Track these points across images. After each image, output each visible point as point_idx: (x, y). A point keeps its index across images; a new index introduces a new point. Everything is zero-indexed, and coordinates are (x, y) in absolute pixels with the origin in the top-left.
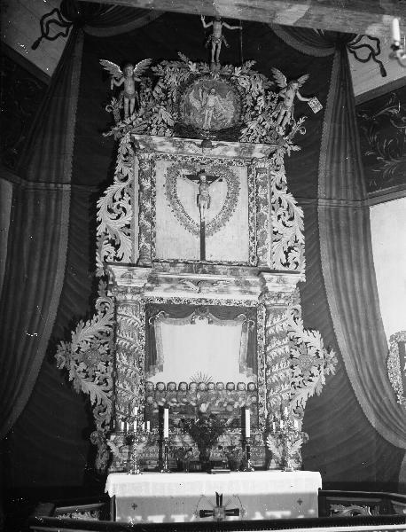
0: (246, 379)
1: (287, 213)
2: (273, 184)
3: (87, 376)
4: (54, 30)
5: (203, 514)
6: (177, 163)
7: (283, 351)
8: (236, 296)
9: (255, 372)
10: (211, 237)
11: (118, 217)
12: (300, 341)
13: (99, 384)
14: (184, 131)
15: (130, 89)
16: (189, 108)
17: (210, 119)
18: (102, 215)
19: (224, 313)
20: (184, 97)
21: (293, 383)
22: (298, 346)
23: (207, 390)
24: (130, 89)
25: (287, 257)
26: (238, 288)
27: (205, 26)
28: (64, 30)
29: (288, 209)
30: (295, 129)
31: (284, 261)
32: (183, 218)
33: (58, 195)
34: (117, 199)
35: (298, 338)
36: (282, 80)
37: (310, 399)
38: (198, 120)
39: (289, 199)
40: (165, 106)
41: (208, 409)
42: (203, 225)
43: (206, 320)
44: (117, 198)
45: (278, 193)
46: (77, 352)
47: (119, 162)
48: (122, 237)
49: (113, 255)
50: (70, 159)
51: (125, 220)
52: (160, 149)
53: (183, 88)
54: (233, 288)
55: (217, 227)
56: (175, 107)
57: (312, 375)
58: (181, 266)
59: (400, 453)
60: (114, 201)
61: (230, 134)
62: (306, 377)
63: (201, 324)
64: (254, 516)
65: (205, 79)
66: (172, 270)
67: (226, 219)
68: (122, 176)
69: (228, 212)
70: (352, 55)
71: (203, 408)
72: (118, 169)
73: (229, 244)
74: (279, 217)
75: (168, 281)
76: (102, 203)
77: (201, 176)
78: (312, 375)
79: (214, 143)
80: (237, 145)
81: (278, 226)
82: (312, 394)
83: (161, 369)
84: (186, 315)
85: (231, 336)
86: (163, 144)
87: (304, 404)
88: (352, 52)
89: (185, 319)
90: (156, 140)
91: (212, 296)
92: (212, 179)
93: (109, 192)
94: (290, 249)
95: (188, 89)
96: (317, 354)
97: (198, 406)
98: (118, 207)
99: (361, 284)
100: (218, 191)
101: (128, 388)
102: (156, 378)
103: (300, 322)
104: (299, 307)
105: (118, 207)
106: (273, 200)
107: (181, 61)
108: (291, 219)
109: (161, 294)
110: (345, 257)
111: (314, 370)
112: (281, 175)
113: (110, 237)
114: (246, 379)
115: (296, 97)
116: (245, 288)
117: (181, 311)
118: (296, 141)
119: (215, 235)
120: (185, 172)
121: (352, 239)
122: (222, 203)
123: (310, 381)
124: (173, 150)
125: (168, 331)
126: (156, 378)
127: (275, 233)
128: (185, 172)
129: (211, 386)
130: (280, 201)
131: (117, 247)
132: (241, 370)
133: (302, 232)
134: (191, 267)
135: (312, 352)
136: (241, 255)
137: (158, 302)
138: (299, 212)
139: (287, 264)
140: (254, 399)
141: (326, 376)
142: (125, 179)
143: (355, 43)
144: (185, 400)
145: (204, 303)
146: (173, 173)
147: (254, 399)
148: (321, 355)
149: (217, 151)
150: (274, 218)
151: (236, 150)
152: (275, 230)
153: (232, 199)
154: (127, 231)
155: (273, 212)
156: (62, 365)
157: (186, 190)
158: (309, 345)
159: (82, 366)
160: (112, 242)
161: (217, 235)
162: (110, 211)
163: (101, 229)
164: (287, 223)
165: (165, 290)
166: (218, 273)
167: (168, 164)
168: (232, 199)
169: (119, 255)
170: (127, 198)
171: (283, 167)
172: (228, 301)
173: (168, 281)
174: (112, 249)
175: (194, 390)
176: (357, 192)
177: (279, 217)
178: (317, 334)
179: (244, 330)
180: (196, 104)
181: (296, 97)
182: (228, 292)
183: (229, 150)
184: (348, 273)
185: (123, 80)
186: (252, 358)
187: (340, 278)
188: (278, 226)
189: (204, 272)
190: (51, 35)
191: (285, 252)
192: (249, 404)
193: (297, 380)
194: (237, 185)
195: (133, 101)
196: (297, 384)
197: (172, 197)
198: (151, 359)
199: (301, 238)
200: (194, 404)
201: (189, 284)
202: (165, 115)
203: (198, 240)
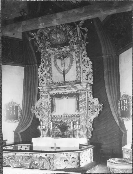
0: (77, 113)
1: (87, 63)
2: (82, 55)
3: (38, 114)
5: (52, 148)
6: (56, 55)
7: (82, 106)
8: (73, 91)
10: (66, 75)
11: (43, 73)
12: (92, 102)
13: (41, 116)
14: (53, 46)
15: (37, 39)
16: (53, 39)
17: (60, 41)
18: (39, 73)
19: (70, 95)
20: (51, 37)
21: (90, 114)
22: (91, 103)
24: (37, 39)
25: (87, 77)
26: (73, 88)
29: (87, 62)
31: (86, 78)
33: (35, 67)
37: (94, 119)
38: (57, 42)
39: (88, 59)
40: (47, 40)
41: (67, 122)
42: (64, 71)
43: (66, 98)
45: (84, 58)
46: (36, 108)
47: (42, 58)
49: (42, 83)
50: (35, 58)
51: (44, 73)
52: (49, 52)
53: (49, 35)
54: (72, 88)
55: (68, 71)
56: (49, 40)
57: (95, 112)
58: (57, 84)
60: (42, 68)
61: (66, 44)
62: (93, 112)
63: (65, 99)
64: (129, 150)
65: (53, 31)
66: (54, 86)
67: (70, 68)
68: (43, 61)
69: (71, 66)
71: (65, 121)
72: (42, 60)
73: (71, 76)
74: (85, 65)
75: (55, 88)
77: (63, 57)
78: (95, 112)
79: (62, 48)
80: (68, 47)
81: (84, 68)
82: (95, 117)
83: (55, 111)
84: (61, 97)
85: (73, 101)
86: (50, 50)
87: (93, 120)
89: (61, 98)
90: (48, 50)
91: (67, 91)
94: (89, 74)
95: (51, 34)
96: (97, 105)
97: (64, 121)
98: (43, 70)
99: (114, 81)
100: (68, 60)
101: (44, 117)
102: (55, 114)
103: (92, 96)
104: (91, 92)
105: (43, 70)
106: (82, 60)
109: (55, 92)
110: (112, 73)
111: (96, 110)
112: (84, 52)
113: (41, 78)
116: (75, 88)
117: (60, 96)
118: (87, 40)
119: (67, 73)
120: (58, 57)
122: (69, 64)
123: (95, 113)
124: (53, 52)
125: (57, 101)
126: (55, 114)
127: (84, 70)
128: (58, 57)
130: (85, 60)
131: (43, 81)
132: (76, 111)
133: (92, 69)
134: (60, 84)
135: (95, 105)
136: (74, 78)
137: (54, 94)
138: (91, 62)
139: (87, 79)
140: (78, 119)
141: (99, 111)
142: (43, 62)
144: (61, 119)
145: (65, 93)
146: (55, 58)
147: (78, 119)
148: (98, 105)
149: (64, 50)
150: (83, 66)
151: (69, 48)
152: (83, 69)
153: (71, 62)
154: (45, 76)
155: (83, 64)
157: (59, 62)
158: (94, 103)
159: (37, 112)
160: (42, 80)
161: (68, 73)
162: (41, 71)
165: (55, 91)
166: (66, 85)
167: (54, 55)
168: (71, 62)
169: (44, 83)
170: (44, 67)
171: (85, 50)
172: (71, 92)
173: (55, 88)
174: (42, 81)
177: (85, 65)
178: (97, 99)
179: (76, 100)
180: (54, 38)
182: (71, 90)
183: (68, 48)
184: (112, 78)
185: (35, 37)
187: (110, 80)
188: (84, 68)
189: (62, 85)
192: (77, 120)
193: (90, 113)
194: (73, 58)
195: (39, 41)
196: (91, 114)
197: (56, 64)
199: (91, 71)
200: (63, 121)
201: (61, 89)
202: (48, 43)
203: (63, 76)
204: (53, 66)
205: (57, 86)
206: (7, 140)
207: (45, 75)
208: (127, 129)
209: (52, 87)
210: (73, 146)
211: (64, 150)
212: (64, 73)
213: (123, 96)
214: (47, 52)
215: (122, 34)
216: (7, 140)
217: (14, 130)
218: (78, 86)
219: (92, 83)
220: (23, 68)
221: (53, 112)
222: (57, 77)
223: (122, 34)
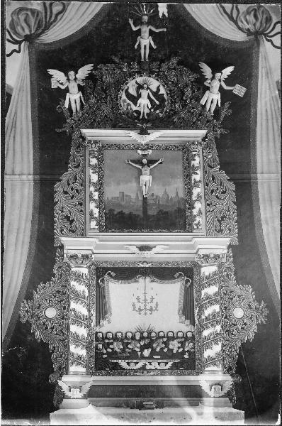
0: (184, 327)
9: (193, 323)
11: (72, 197)
19: (162, 273)
27: (134, 29)
28: (16, 47)
30: (223, 113)
34: (71, 183)
35: (231, 292)
36: (207, 71)
59: (4, 417)
60: (69, 184)
70: (269, 43)
76: (58, 187)
85: (172, 292)
88: (268, 40)
93: (64, 178)
96: (249, 306)
107: (115, 63)
114: (184, 327)
115: (221, 86)
117: (127, 273)
121: (267, 205)
125: (117, 291)
126: (107, 327)
129: (153, 334)
131: (72, 222)
138: (231, 186)
143: (269, 33)
156: (246, 339)
175: (138, 338)
181: (221, 86)
186: (189, 308)
191: (218, 220)
198: (102, 310)
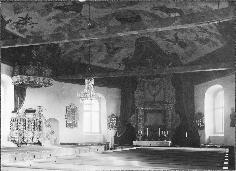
4: (122, 65)
23: (156, 126)
32: (151, 94)
44: (138, 91)
48: (139, 98)
51: (140, 95)
54: (160, 106)
55: (157, 95)
92: (156, 85)
94: (172, 98)
100: (158, 86)
108: (173, 91)
111: (178, 122)
134: (151, 103)
138: (174, 90)
157: (151, 88)
163: (135, 97)
164: (172, 92)
170: (139, 91)
176: (124, 109)
179: (163, 115)
182: (160, 107)
190: (122, 65)
198: (95, 133)
204: (146, 91)
205: (149, 104)
206: (109, 143)
207: (140, 96)
208: (200, 135)
209: (146, 105)
210: (28, 165)
211: (33, 167)
212: (154, 96)
213: (197, 113)
214: (143, 81)
215: (90, 69)
216: (109, 143)
217: (114, 136)
218: (166, 105)
219: (175, 103)
220: (121, 89)
221: (145, 122)
222: (149, 97)
223: (90, 69)
